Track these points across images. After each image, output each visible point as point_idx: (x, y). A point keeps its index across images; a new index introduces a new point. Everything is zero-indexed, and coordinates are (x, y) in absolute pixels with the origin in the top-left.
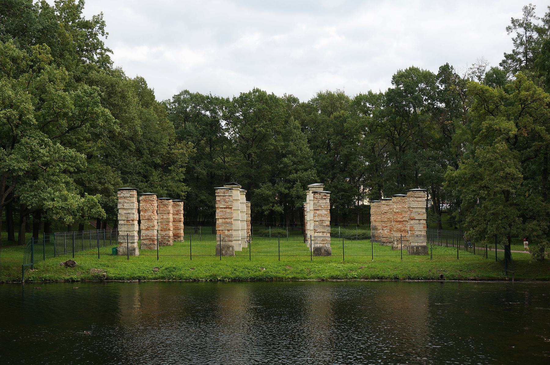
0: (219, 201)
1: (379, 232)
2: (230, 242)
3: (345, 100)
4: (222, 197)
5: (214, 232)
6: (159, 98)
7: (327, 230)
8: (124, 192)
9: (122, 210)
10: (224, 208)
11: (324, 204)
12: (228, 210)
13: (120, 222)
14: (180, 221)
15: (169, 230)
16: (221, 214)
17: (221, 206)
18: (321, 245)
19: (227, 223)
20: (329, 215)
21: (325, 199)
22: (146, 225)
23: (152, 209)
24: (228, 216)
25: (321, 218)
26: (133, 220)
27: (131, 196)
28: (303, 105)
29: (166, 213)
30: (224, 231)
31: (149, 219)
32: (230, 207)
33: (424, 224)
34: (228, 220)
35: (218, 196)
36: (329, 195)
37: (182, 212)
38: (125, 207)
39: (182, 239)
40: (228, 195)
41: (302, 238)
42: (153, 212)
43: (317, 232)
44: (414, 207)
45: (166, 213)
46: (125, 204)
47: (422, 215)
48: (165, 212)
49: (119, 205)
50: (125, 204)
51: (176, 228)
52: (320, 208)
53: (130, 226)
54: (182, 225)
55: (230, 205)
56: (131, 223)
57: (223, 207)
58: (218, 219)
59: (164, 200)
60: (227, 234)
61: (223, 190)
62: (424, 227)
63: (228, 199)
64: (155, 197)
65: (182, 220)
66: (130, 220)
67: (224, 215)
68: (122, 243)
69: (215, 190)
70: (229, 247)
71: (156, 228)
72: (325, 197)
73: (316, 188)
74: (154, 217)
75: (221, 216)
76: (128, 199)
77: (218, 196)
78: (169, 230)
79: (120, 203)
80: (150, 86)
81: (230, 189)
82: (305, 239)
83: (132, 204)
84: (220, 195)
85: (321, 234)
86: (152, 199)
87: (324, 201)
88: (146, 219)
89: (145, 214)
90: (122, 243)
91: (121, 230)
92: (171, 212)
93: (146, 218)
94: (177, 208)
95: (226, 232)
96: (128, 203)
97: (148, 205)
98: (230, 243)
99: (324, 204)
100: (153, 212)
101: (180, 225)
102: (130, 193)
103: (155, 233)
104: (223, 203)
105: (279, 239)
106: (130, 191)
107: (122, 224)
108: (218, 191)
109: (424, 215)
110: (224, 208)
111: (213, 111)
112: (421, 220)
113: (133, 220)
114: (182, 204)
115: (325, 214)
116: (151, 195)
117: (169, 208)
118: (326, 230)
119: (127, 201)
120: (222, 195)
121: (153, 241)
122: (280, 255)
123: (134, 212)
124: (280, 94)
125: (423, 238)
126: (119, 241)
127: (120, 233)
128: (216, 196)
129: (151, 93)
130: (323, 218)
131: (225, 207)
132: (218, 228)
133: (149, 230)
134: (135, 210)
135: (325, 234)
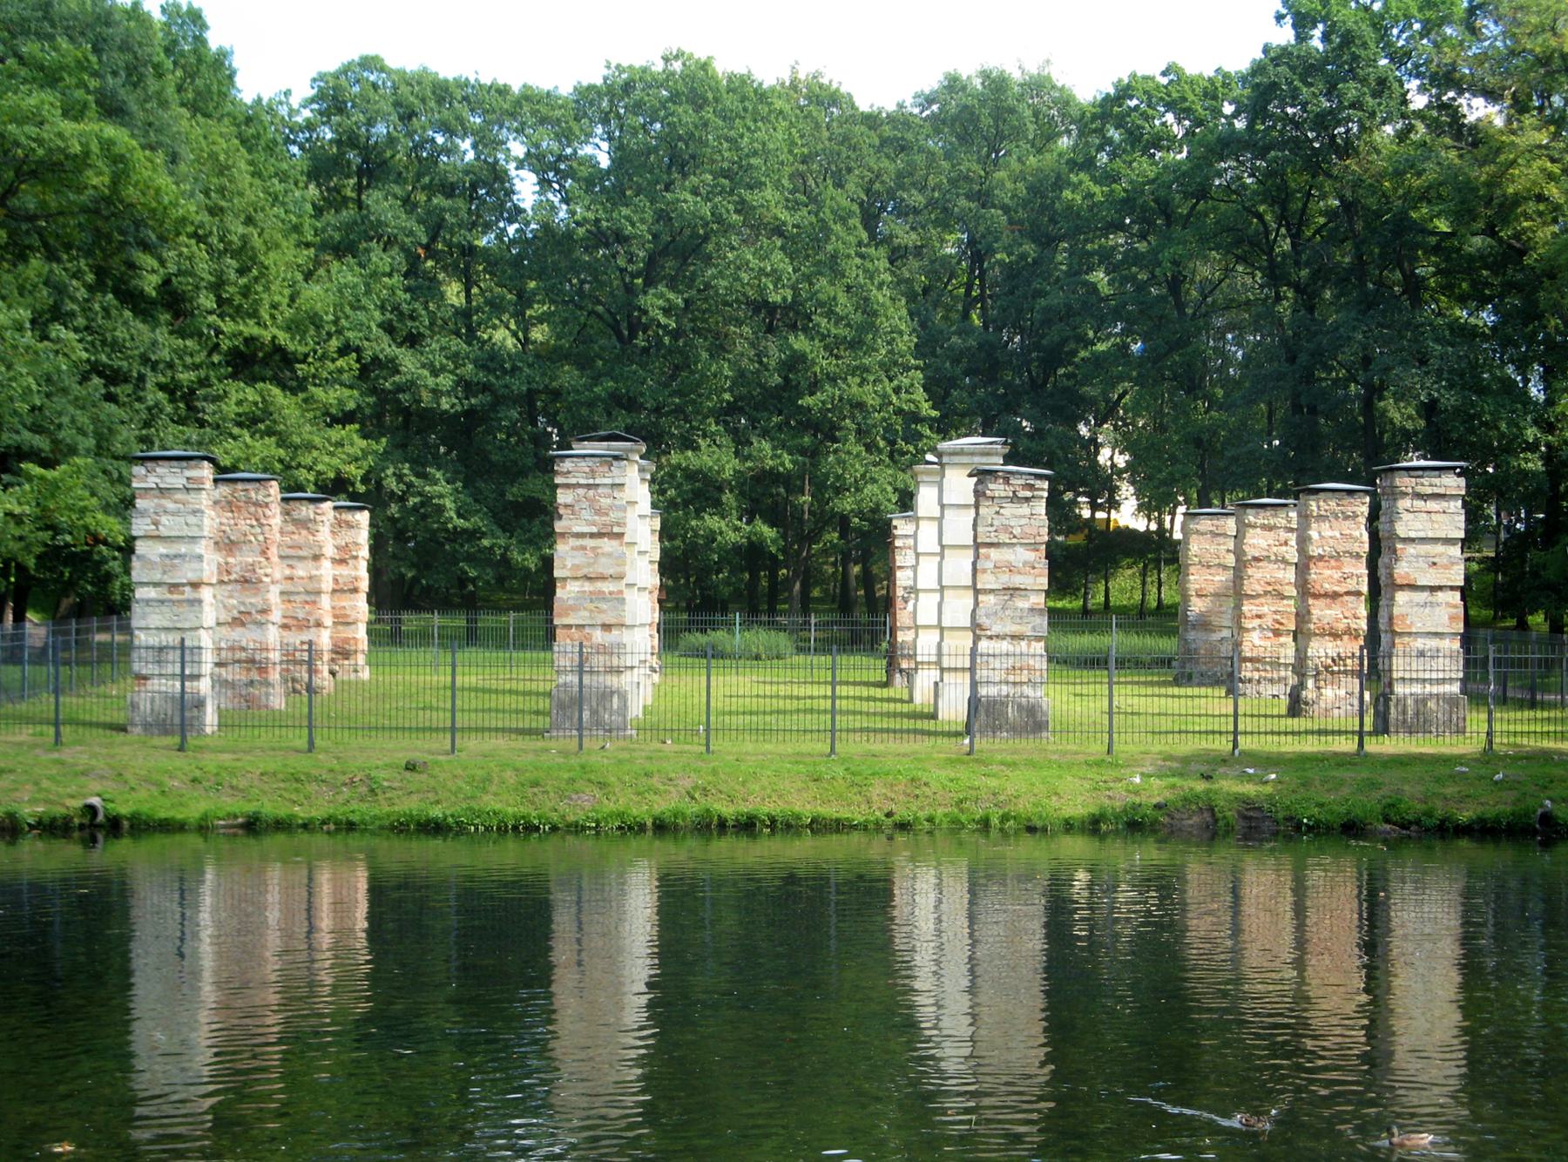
0: (566, 506)
1: (1216, 636)
2: (608, 677)
3: (459, 94)
4: (581, 491)
5: (548, 637)
6: (251, 86)
7: (1034, 629)
8: (162, 469)
9: (150, 543)
10: (592, 535)
11: (1023, 521)
12: (607, 545)
13: (140, 593)
14: (355, 590)
15: (319, 625)
16: (577, 561)
17: (576, 529)
18: (1005, 689)
19: (600, 596)
20: (1043, 566)
21: (1027, 499)
22: (234, 607)
23: (261, 538)
24: (604, 567)
25: (1005, 579)
26: (195, 585)
27: (193, 487)
28: (871, 120)
29: (304, 558)
30: (587, 630)
31: (246, 581)
32: (616, 530)
33: (1455, 607)
34: (607, 587)
35: (567, 486)
36: (1046, 485)
37: (365, 553)
38: (163, 531)
39: (361, 659)
40: (609, 481)
41: (878, 662)
42: (263, 553)
43: (990, 638)
44: (1413, 535)
45: (304, 558)
46: (164, 519)
47: (1446, 567)
48: (301, 553)
49: (139, 521)
50: (164, 519)
51: (342, 620)
52: (1004, 538)
53: (185, 608)
54: (360, 607)
55: (619, 524)
56: (186, 596)
57: (586, 529)
58: (565, 579)
59: (297, 504)
60: (600, 640)
61: (590, 462)
62: (1452, 618)
63: (609, 501)
64: (274, 488)
65: (364, 585)
66: (183, 585)
67: (589, 565)
68: (145, 678)
69: (552, 460)
70: (606, 695)
71: (276, 616)
72: (1029, 494)
73: (972, 454)
74: (269, 571)
75: (576, 567)
76: (179, 496)
77: (567, 486)
78: (319, 625)
79: (143, 514)
80: (215, 40)
81: (616, 458)
82: (890, 664)
83: (192, 519)
84: (573, 481)
85: (1004, 646)
86: (260, 497)
87: (1025, 509)
88: (236, 581)
89: (231, 560)
90: (145, 678)
91: (142, 624)
92: (329, 551)
93: (233, 577)
94: (346, 537)
95: (598, 636)
96: (173, 514)
97: (243, 525)
98: (612, 681)
99: (1023, 521)
100: (263, 553)
101: (354, 608)
102: (188, 473)
103: (813, 621)
104: (586, 514)
105: (708, 668)
106: (184, 464)
107: (148, 602)
108: (567, 465)
109: (1456, 567)
110: (592, 535)
111: (485, 142)
112: (1441, 588)
113: (195, 585)
114: (363, 518)
115: (1025, 563)
116: (258, 480)
117: (320, 537)
118: (1026, 630)
119: (170, 506)
120: (582, 481)
121: (263, 669)
122: (1240, 712)
123: (202, 552)
124: (769, 73)
125: (1447, 661)
126: (136, 667)
127: (142, 638)
128: (557, 486)
129: (220, 67)
130: (1018, 581)
131: (594, 530)
132: (560, 615)
133: (243, 624)
134: (204, 542)
135: (1024, 644)
